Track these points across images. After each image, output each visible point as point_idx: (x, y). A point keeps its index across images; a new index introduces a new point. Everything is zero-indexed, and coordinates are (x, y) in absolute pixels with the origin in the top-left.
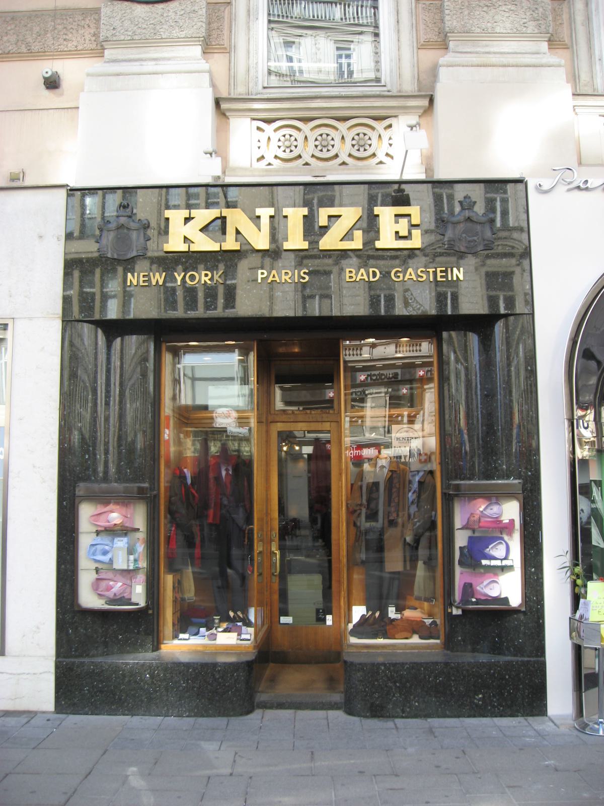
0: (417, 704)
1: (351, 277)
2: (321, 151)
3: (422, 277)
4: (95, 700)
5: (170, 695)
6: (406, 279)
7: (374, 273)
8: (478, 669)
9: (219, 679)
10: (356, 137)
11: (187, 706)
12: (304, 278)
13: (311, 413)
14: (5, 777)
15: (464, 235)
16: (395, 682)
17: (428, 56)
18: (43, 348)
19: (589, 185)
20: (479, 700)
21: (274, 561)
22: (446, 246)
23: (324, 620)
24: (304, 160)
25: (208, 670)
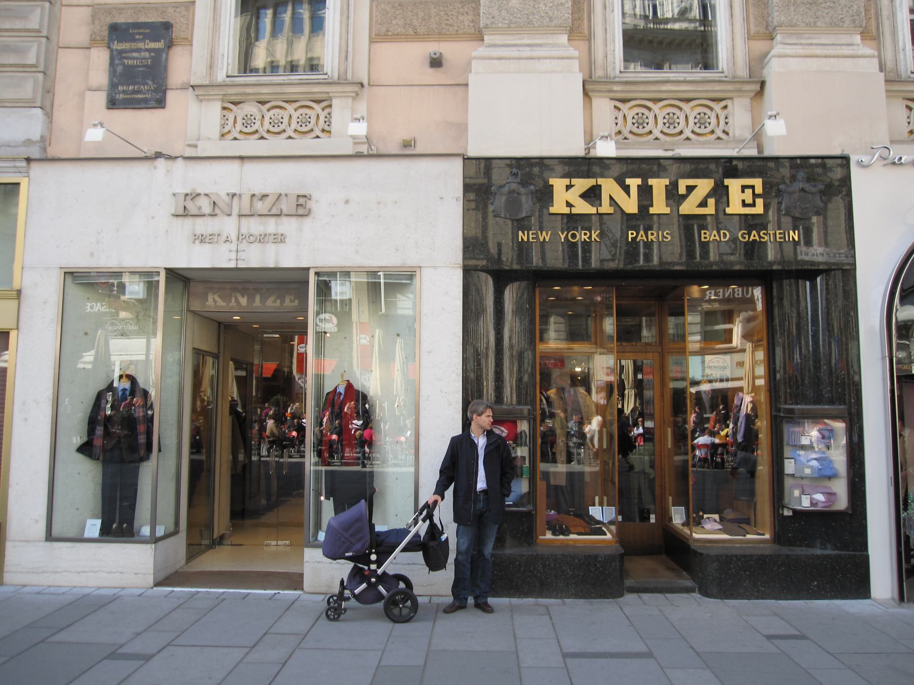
1: (705, 238)
2: (669, 127)
7: (725, 235)
10: (698, 116)
11: (573, 591)
12: (667, 238)
13: (636, 345)
14: (692, 648)
15: (798, 203)
16: (745, 571)
17: (759, 46)
18: (447, 292)
19: (903, 161)
23: (649, 518)
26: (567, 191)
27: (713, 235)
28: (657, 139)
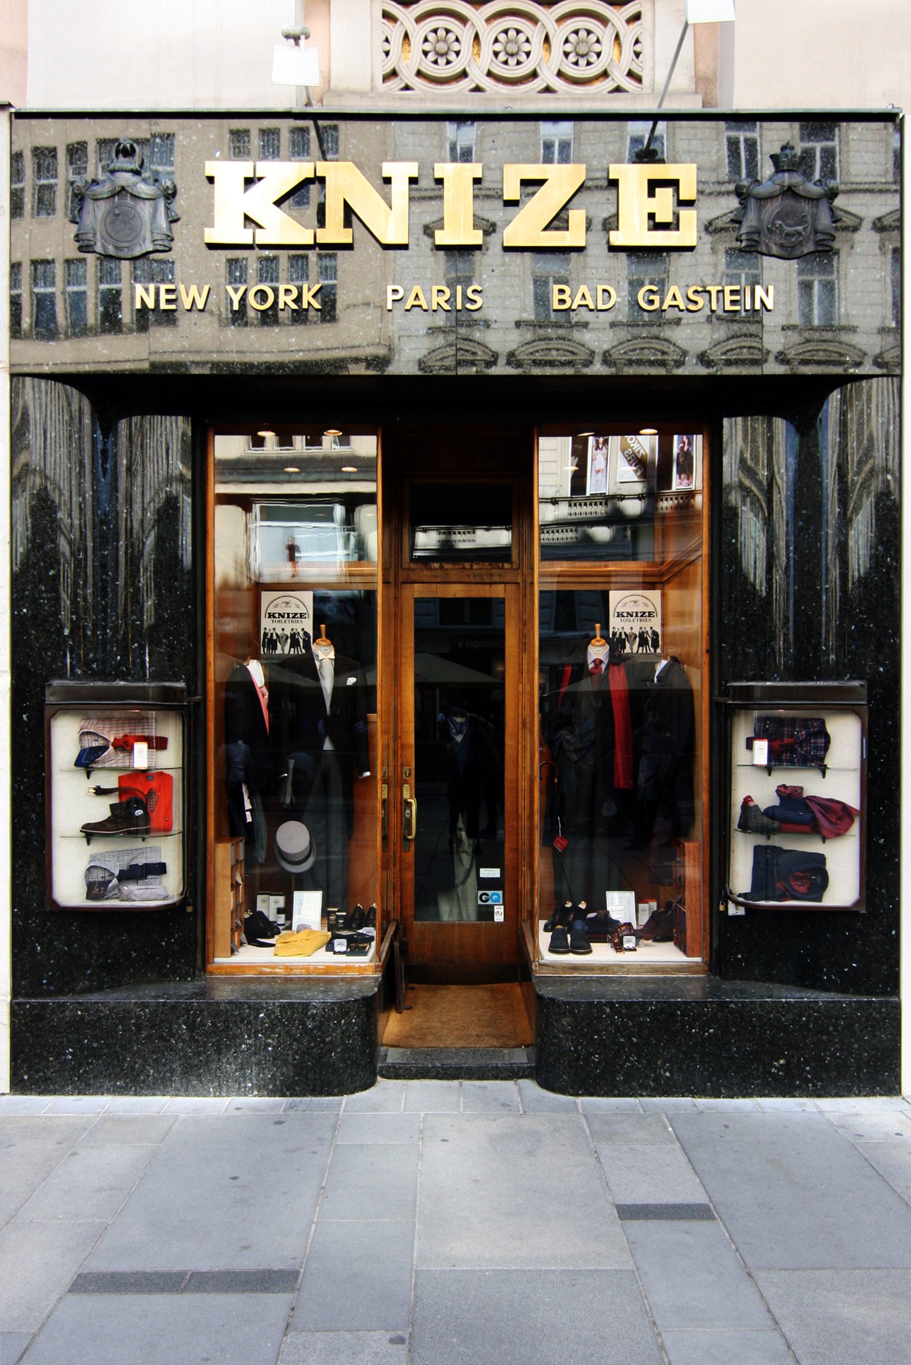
0: (668, 1074)
1: (562, 301)
3: (696, 303)
4: (85, 1071)
5: (224, 1060)
6: (665, 307)
8: (778, 1015)
9: (312, 1030)
13: (471, 568)
20: (780, 1068)
21: (407, 816)
22: (744, 244)
24: (473, 81)
25: (293, 1013)
26: (246, 190)
27: (579, 295)
28: (477, 89)
